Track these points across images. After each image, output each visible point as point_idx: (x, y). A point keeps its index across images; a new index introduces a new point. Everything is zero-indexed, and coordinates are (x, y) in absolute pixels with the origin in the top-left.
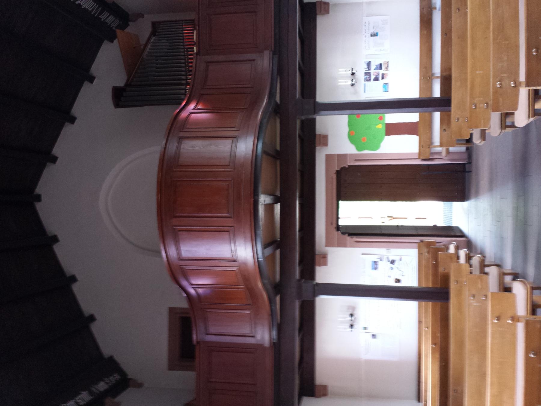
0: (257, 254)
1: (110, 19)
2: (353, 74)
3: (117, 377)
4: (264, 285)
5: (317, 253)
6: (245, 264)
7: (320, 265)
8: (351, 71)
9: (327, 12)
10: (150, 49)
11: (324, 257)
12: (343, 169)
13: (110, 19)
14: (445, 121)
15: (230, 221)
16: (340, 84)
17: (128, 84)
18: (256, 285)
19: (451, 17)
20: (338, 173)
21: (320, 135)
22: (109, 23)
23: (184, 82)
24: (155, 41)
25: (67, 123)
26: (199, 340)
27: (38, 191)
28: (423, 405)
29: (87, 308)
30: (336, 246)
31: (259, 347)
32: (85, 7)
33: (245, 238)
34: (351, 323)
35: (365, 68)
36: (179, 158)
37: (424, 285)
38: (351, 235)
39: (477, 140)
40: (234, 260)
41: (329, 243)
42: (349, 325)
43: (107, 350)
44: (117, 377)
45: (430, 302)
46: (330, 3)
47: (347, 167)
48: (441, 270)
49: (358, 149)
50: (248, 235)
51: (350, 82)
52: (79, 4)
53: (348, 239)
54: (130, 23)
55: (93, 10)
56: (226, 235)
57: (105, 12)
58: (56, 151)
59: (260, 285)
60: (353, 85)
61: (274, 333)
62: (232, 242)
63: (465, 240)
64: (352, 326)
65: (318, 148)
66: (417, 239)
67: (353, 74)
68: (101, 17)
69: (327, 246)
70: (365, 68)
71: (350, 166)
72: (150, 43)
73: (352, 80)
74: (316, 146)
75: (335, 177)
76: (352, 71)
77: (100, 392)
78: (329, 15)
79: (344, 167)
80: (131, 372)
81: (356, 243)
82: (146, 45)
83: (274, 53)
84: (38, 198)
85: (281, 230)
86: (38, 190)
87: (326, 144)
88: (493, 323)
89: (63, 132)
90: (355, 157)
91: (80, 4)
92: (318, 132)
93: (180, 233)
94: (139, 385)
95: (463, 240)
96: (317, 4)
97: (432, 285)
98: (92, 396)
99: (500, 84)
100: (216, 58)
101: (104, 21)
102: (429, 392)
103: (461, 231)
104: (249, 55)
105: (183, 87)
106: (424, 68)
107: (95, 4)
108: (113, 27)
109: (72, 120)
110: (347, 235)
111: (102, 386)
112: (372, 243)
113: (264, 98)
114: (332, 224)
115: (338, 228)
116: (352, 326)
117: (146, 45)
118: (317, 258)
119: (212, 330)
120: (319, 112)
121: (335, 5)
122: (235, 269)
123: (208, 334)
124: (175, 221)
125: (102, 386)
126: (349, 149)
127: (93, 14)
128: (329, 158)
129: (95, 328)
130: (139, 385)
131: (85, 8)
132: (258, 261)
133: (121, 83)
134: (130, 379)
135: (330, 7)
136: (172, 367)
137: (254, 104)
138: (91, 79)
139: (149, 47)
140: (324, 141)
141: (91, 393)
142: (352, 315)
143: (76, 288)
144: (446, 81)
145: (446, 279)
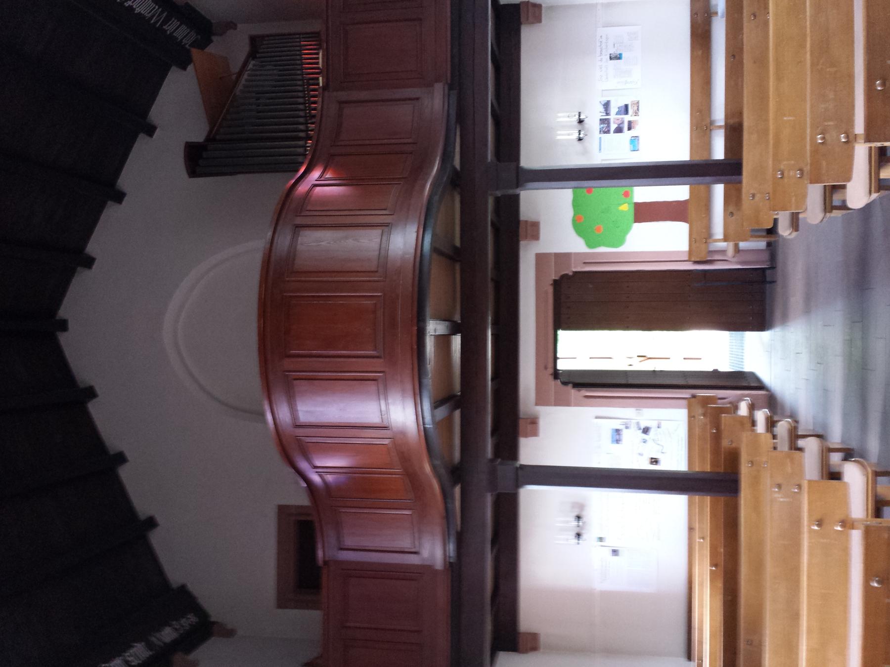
0: (423, 418)
1: (180, 32)
2: (581, 121)
3: (192, 619)
4: (434, 468)
5: (522, 415)
6: (403, 433)
7: (526, 436)
8: (577, 117)
9: (538, 19)
10: (246, 80)
11: (534, 422)
12: (564, 277)
13: (180, 32)
14: (732, 199)
15: (378, 364)
16: (559, 137)
17: (210, 139)
18: (422, 468)
19: (741, 29)
20: (556, 284)
21: (526, 222)
22: (180, 38)
23: (302, 134)
24: (255, 67)
25: (109, 203)
26: (327, 559)
27: (62, 313)
28: (695, 666)
29: (143, 506)
30: (553, 403)
31: (426, 570)
32: (140, 12)
33: (403, 391)
34: (577, 530)
35: (600, 112)
36: (294, 260)
37: (697, 469)
38: (578, 385)
39: (784, 231)
40: (385, 428)
41: (542, 399)
42: (573, 533)
43: (175, 576)
44: (192, 619)
45: (708, 496)
46: (543, 5)
47: (571, 274)
48: (725, 443)
49: (589, 245)
50: (409, 386)
51: (576, 135)
52: (131, 7)
53: (573, 392)
54: (214, 38)
55: (153, 16)
56: (372, 386)
57: (173, 19)
58: (93, 248)
59: (427, 468)
60: (580, 139)
61: (452, 548)
62: (382, 397)
63: (764, 395)
64: (578, 535)
65: (523, 243)
66: (686, 393)
67: (581, 121)
68: (167, 29)
69: (538, 403)
70: (600, 112)
71: (576, 273)
72: (246, 71)
73: (580, 131)
74: (520, 239)
75: (550, 290)
76: (579, 116)
77: (165, 644)
78: (540, 24)
79: (566, 275)
80: (215, 610)
81: (586, 400)
82: (240, 74)
83: (451, 87)
84: (63, 325)
85: (462, 378)
86: (63, 312)
87: (536, 236)
88: (811, 531)
89: (103, 217)
90: (585, 258)
91: (132, 6)
92: (523, 217)
93: (295, 382)
94: (229, 633)
95: (761, 395)
96: (521, 7)
97: (710, 468)
98: (151, 650)
99: (823, 138)
100: (356, 95)
101: (170, 34)
102: (706, 643)
103: (758, 379)
104: (409, 90)
105: (301, 143)
106: (698, 112)
107: (157, 7)
108: (185, 44)
109: (119, 197)
110: (570, 386)
111: (168, 635)
112: (612, 400)
113: (435, 160)
114: (546, 368)
115: (556, 374)
116: (578, 535)
117: (240, 74)
118: (522, 424)
119: (349, 542)
120: (525, 184)
121: (551, 8)
122: (386, 442)
123: (342, 549)
124: (287, 363)
125: (168, 635)
126: (575, 244)
127: (153, 23)
128: (541, 259)
129: (156, 538)
130: (229, 633)
131: (140, 14)
132: (425, 428)
133: (199, 136)
134: (214, 623)
135: (543, 11)
136: (282, 602)
137: (418, 171)
138: (150, 130)
139: (245, 77)
140: (534, 231)
141: (150, 646)
142: (579, 518)
143: (125, 473)
144: (734, 133)
145: (733, 458)
